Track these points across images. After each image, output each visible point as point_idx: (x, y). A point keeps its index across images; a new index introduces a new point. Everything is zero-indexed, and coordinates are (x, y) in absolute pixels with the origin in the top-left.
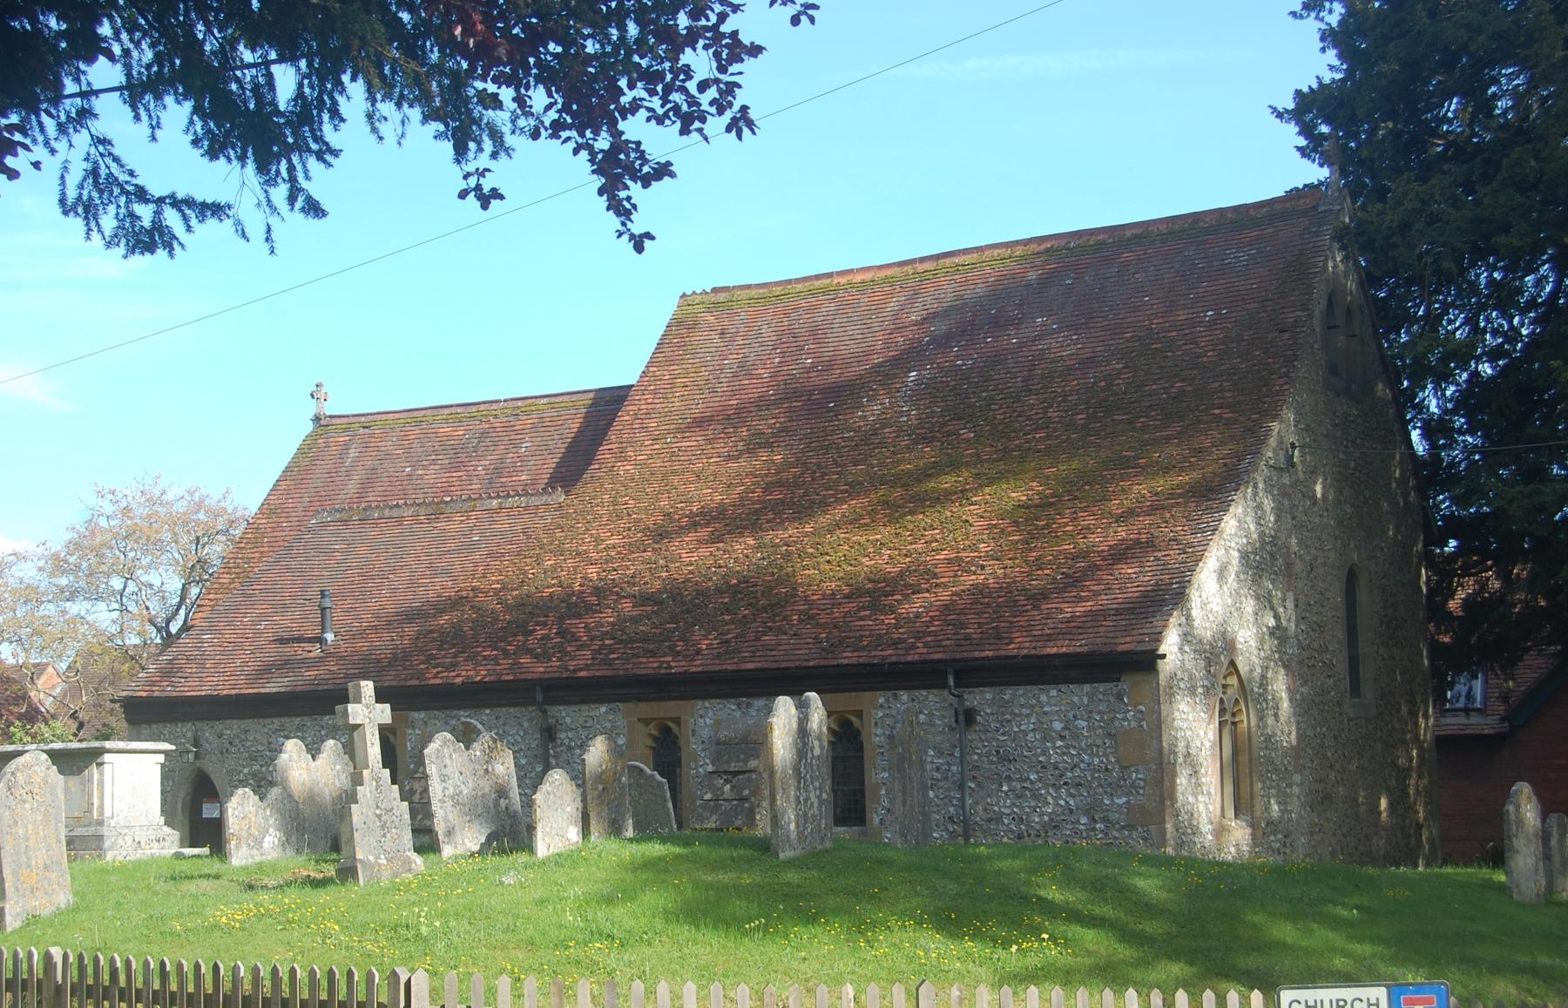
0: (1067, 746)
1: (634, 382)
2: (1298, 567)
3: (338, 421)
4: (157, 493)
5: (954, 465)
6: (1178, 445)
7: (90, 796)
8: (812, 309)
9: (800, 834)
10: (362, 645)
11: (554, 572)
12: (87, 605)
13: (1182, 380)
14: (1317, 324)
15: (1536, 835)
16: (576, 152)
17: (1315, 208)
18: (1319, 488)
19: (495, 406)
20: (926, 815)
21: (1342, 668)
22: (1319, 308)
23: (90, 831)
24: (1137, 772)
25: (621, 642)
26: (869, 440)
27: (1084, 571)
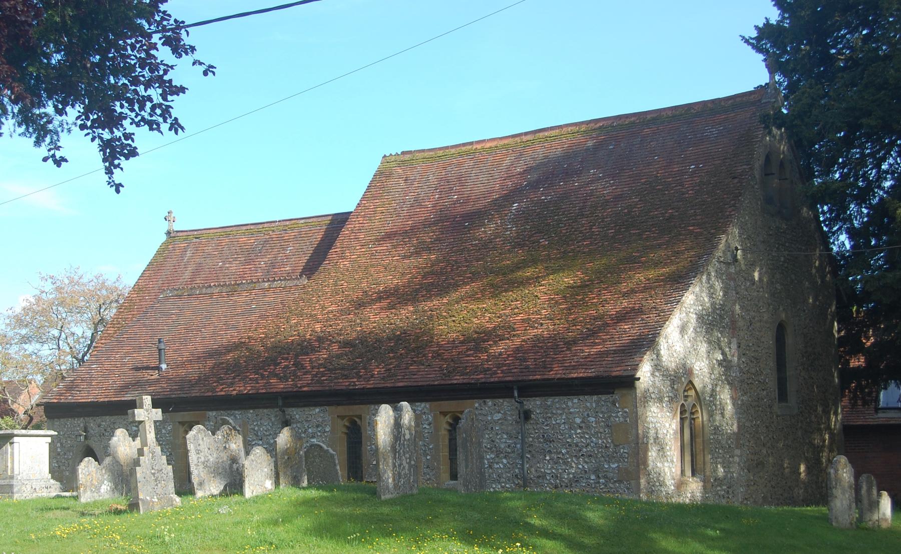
0: (584, 433)
1: (352, 210)
2: (741, 323)
3: (181, 234)
4: (76, 278)
5: (534, 262)
6: (666, 249)
7: (6, 461)
8: (459, 165)
9: (396, 486)
10: (182, 372)
12: (38, 346)
13: (672, 209)
14: (757, 173)
15: (850, 487)
16: (93, 140)
17: (760, 101)
18: (756, 275)
19: (273, 225)
21: (772, 383)
22: (758, 164)
23: (6, 482)
24: (624, 448)
25: (329, 370)
26: (486, 245)
27: (599, 327)
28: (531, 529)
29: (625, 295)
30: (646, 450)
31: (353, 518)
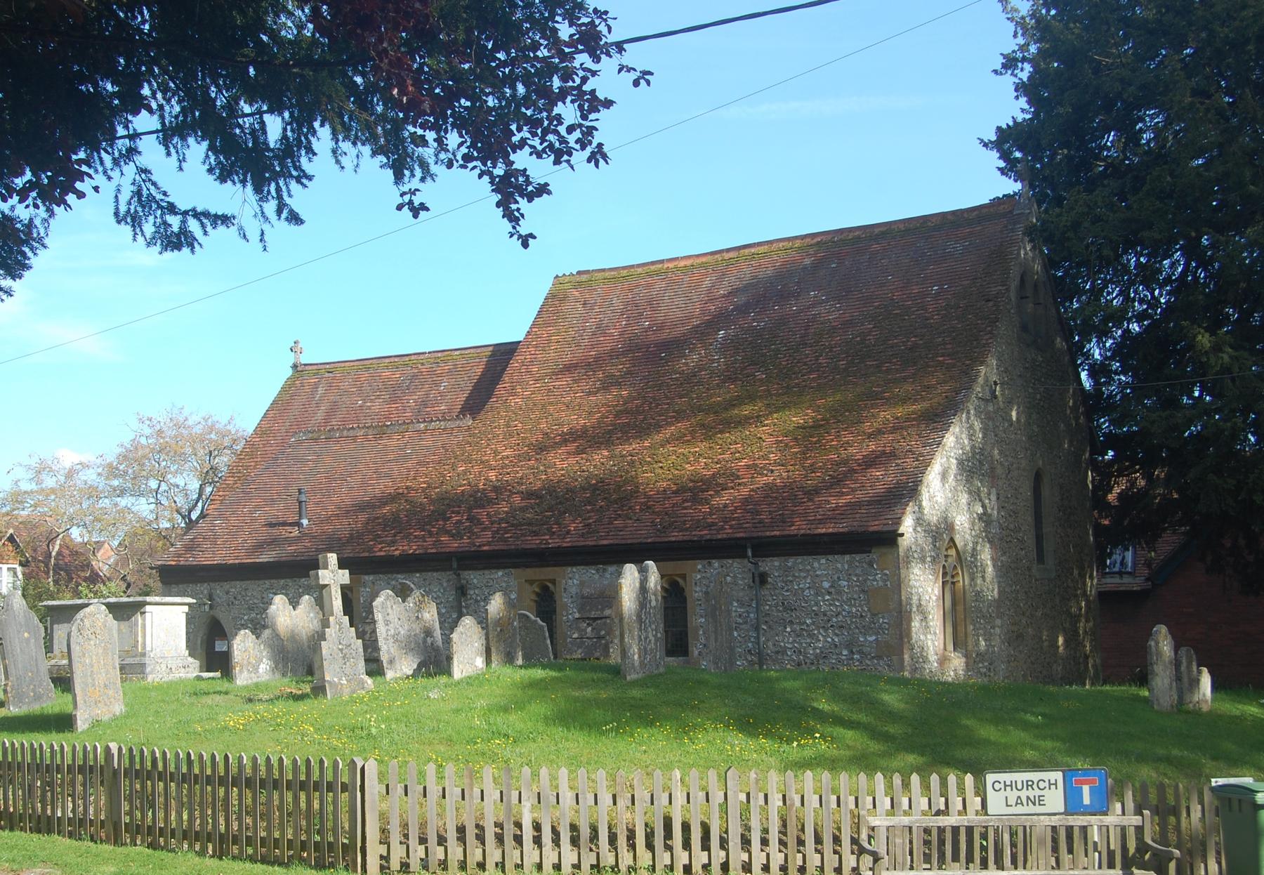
2: (999, 471)
4: (181, 419)
5: (752, 398)
8: (649, 286)
9: (642, 663)
10: (329, 528)
11: (465, 476)
12: (132, 499)
14: (1013, 295)
17: (1011, 212)
18: (1014, 414)
20: (732, 649)
21: (1030, 541)
22: (1014, 285)
25: (513, 525)
26: (690, 379)
27: (845, 474)
28: (821, 716)
29: (870, 436)
30: (910, 620)
31: (598, 703)
